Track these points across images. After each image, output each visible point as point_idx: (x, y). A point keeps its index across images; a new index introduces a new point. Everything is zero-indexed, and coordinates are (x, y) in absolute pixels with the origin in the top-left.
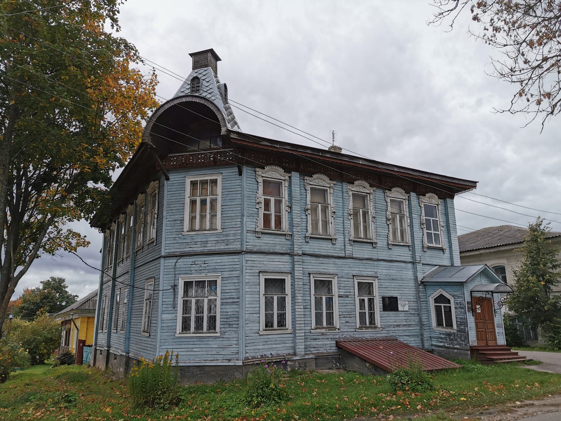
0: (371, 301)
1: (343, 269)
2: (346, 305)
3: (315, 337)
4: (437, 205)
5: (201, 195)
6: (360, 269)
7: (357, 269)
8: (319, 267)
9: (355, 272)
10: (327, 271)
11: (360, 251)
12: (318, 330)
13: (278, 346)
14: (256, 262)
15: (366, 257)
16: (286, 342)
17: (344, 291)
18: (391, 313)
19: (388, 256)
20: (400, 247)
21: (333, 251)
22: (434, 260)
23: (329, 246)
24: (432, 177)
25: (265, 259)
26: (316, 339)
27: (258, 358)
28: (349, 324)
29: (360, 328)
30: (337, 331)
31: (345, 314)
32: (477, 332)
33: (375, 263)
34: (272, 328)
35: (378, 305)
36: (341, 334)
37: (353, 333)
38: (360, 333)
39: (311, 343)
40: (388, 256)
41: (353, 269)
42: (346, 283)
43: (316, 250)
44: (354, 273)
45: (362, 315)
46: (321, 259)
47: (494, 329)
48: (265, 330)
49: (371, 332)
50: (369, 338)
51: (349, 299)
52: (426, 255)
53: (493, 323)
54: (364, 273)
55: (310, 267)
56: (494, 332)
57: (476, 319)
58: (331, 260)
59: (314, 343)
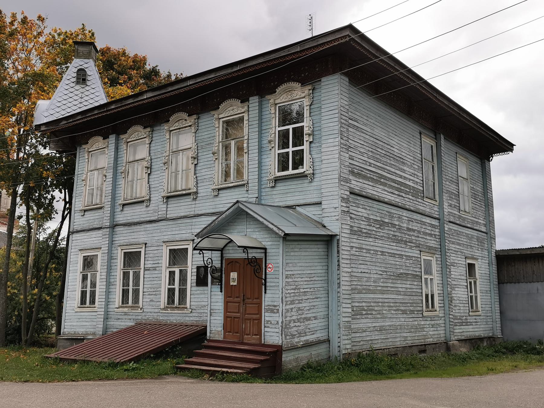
0: (183, 274)
1: (154, 235)
2: (153, 279)
3: (119, 317)
4: (276, 104)
5: (294, 145)
6: (174, 233)
7: (169, 233)
8: (130, 237)
9: (167, 237)
10: (136, 240)
11: (176, 208)
12: (121, 309)
13: (87, 324)
14: (78, 241)
15: (182, 214)
16: (93, 320)
17: (152, 262)
18: (201, 288)
19: (212, 207)
20: (233, 190)
21: (145, 216)
22: (288, 199)
23: (143, 210)
24: (321, 41)
25: (85, 237)
26: (119, 319)
27: (72, 334)
28: (154, 303)
29: (165, 308)
30: (139, 311)
31: (151, 290)
32: (226, 317)
33: (194, 220)
34: (85, 306)
35: (191, 278)
36: (144, 314)
37: (156, 314)
38: (166, 315)
39: (115, 323)
40: (212, 207)
41: (165, 234)
42: (156, 252)
43: (129, 218)
44: (166, 238)
45: (171, 292)
46: (133, 227)
47: (259, 312)
48: (121, 307)
49: (178, 315)
50: (175, 321)
51: (156, 272)
52: (275, 193)
53: (260, 304)
54: (178, 238)
55: (122, 238)
56: (260, 319)
57: (226, 296)
58: (143, 226)
59: (117, 323)
